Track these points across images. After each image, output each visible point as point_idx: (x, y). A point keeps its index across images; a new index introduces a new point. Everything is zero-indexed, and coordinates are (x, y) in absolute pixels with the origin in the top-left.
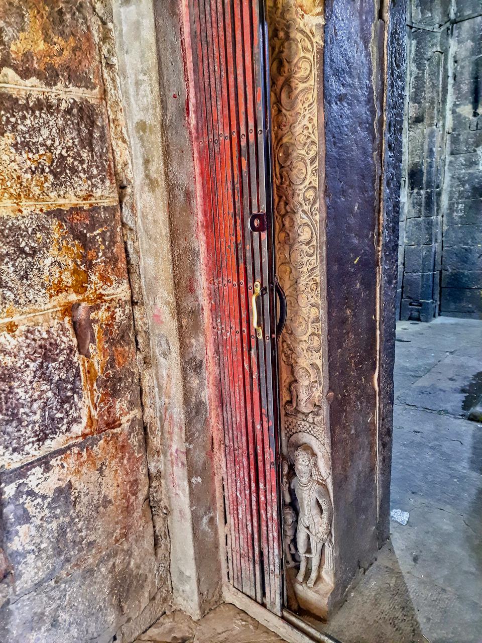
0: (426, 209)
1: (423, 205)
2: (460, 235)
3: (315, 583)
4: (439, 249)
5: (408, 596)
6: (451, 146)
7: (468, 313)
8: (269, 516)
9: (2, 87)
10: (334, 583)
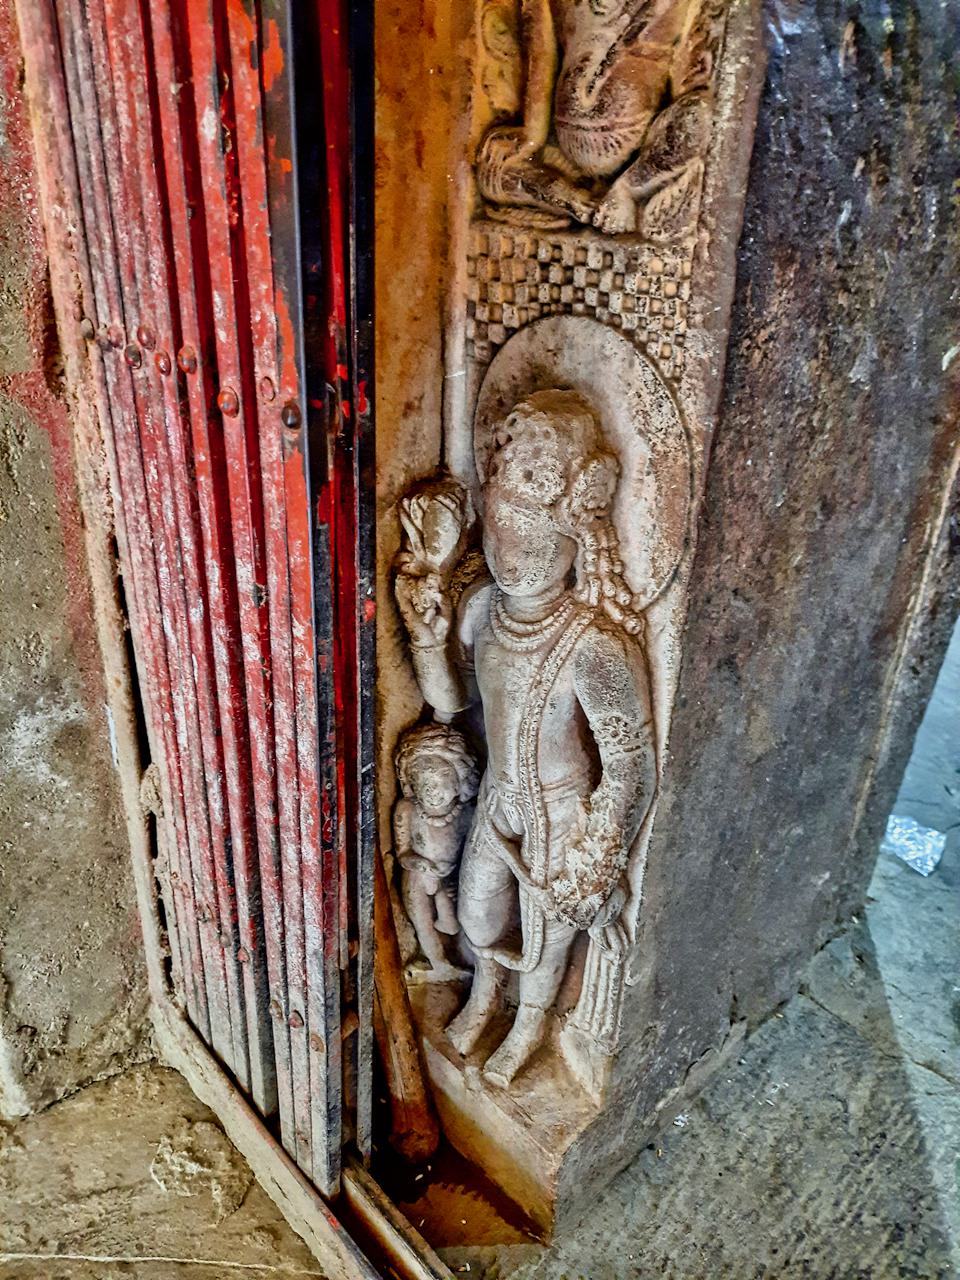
3: (521, 1073)
5: (923, 1175)
8: (282, 751)
10: (605, 1093)
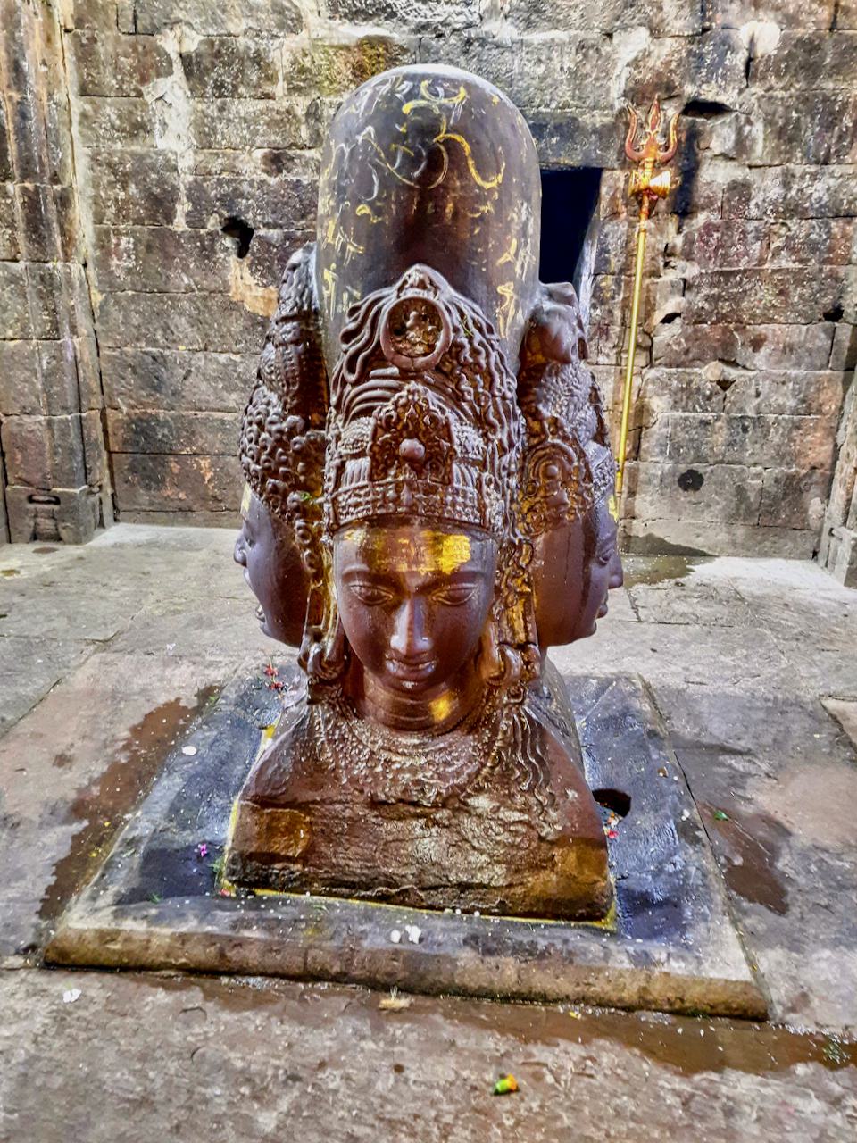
0: (30, 239)
1: (21, 225)
2: (136, 319)
4: (87, 355)
6: (78, 69)
7: (183, 513)
9: (854, 699)
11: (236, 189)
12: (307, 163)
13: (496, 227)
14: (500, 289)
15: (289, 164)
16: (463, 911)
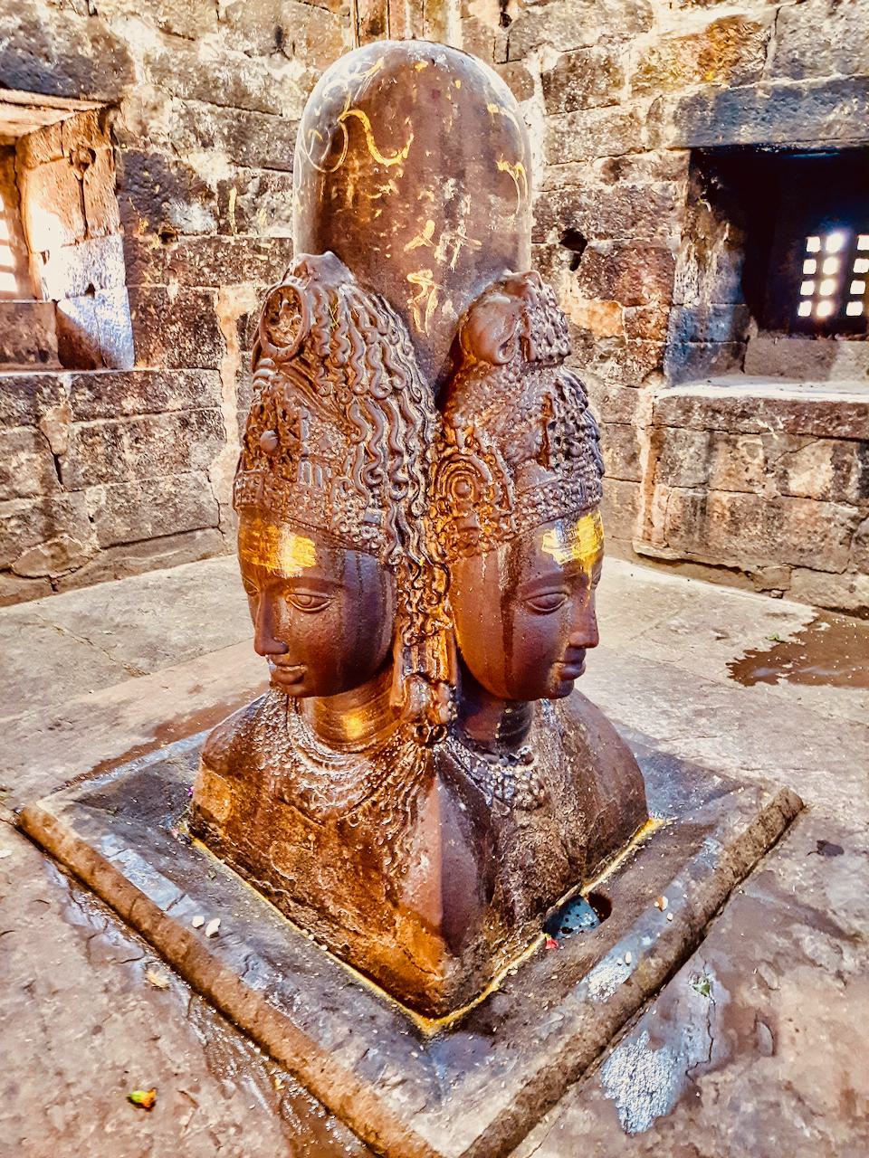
11: (576, 201)
12: (644, 166)
13: (403, 209)
14: (411, 277)
15: (626, 170)
16: (315, 939)
